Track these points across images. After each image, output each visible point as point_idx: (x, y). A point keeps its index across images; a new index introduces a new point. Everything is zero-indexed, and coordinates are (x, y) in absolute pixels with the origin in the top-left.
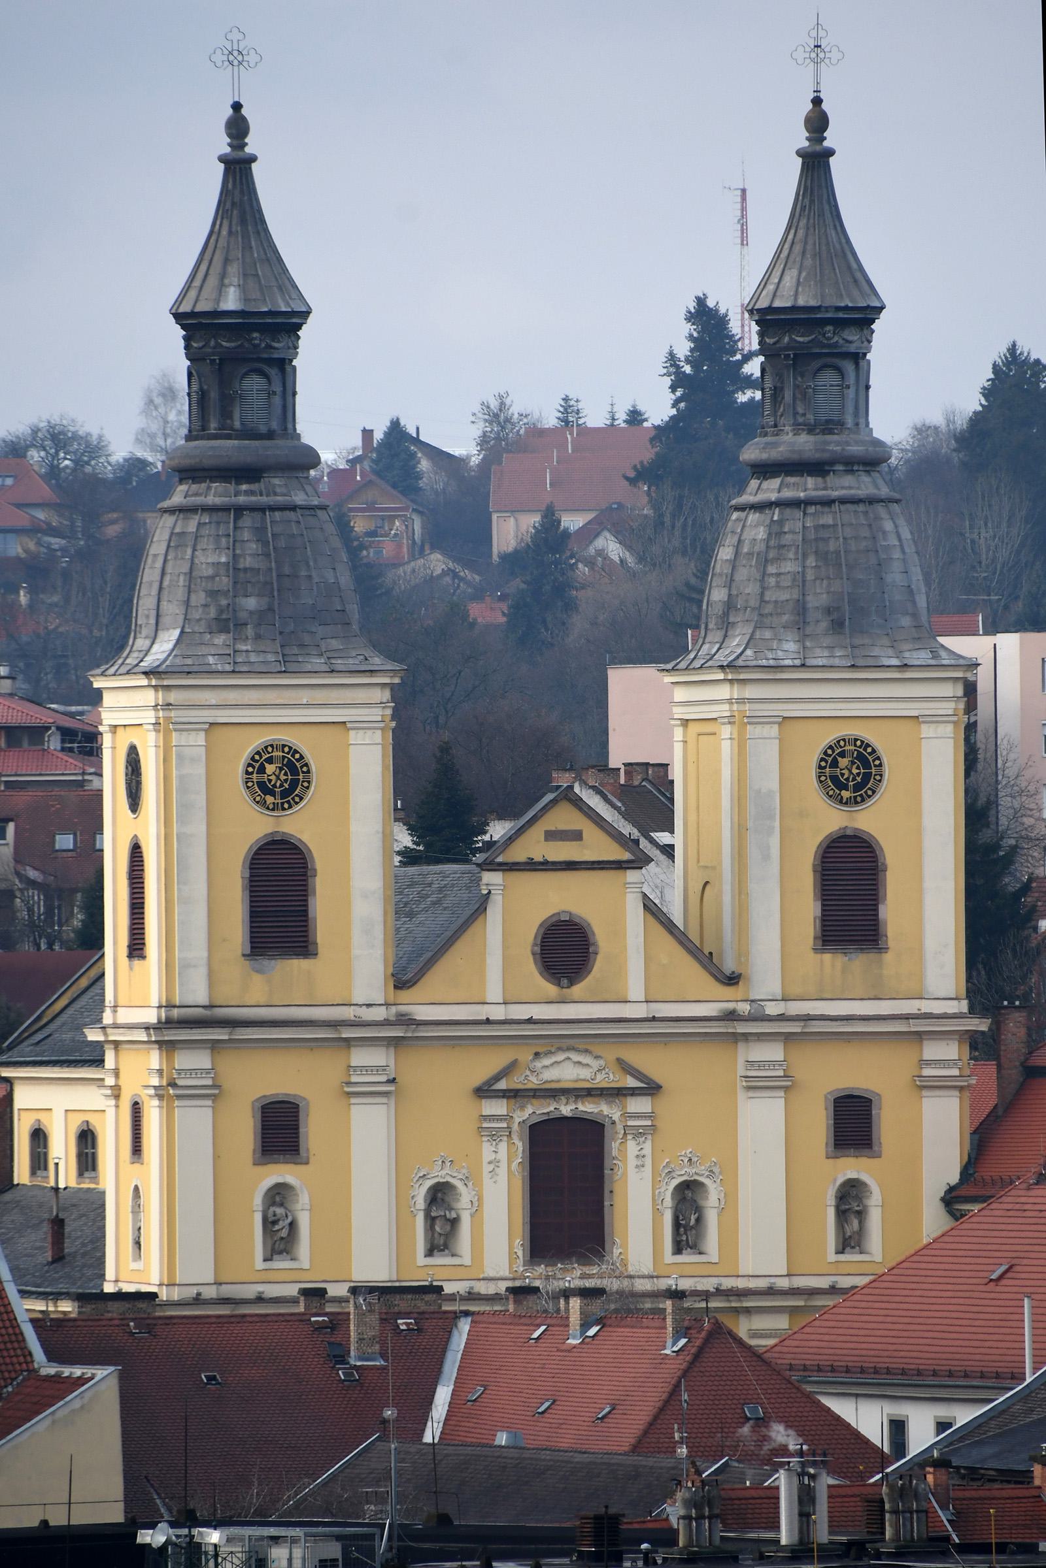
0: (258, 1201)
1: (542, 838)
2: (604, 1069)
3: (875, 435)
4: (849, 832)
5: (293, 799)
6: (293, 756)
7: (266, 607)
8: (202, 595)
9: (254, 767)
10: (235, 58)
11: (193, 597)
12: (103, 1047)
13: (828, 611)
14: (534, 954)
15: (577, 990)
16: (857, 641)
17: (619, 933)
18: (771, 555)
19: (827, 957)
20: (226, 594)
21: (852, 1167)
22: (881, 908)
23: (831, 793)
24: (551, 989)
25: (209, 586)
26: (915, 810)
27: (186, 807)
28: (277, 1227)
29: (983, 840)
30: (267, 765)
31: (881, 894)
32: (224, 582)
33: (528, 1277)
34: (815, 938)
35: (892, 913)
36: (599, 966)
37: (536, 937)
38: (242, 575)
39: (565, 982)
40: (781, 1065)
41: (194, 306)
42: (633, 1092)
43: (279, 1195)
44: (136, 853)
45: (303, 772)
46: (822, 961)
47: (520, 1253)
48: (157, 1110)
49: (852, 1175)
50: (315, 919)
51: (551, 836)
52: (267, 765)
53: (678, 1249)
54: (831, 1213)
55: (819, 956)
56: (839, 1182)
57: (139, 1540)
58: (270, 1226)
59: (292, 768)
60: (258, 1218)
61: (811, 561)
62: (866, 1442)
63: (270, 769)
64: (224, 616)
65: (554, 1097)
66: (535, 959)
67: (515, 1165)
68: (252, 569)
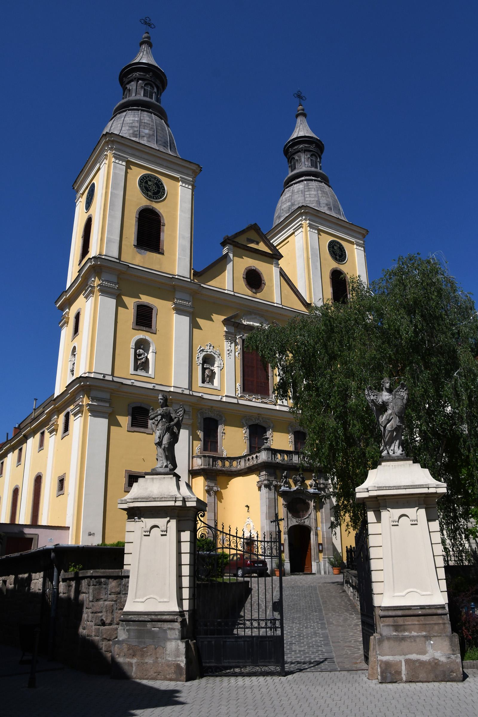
0: (132, 344)
7: (152, 134)
8: (127, 128)
10: (147, 23)
11: (123, 128)
13: (327, 205)
14: (243, 278)
17: (271, 280)
18: (306, 190)
20: (137, 127)
21: (141, 335)
23: (144, 192)
24: (249, 292)
25: (130, 125)
28: (140, 357)
29: (33, 590)
30: (149, 181)
32: (137, 124)
36: (265, 288)
38: (143, 124)
39: (254, 290)
41: (110, 130)
43: (142, 345)
44: (38, 480)
47: (239, 389)
48: (122, 631)
49: (141, 336)
50: (163, 241)
52: (149, 181)
58: (137, 356)
60: (132, 352)
61: (319, 192)
62: (201, 500)
63: (149, 183)
64: (136, 133)
66: (244, 280)
67: (237, 353)
68: (147, 123)
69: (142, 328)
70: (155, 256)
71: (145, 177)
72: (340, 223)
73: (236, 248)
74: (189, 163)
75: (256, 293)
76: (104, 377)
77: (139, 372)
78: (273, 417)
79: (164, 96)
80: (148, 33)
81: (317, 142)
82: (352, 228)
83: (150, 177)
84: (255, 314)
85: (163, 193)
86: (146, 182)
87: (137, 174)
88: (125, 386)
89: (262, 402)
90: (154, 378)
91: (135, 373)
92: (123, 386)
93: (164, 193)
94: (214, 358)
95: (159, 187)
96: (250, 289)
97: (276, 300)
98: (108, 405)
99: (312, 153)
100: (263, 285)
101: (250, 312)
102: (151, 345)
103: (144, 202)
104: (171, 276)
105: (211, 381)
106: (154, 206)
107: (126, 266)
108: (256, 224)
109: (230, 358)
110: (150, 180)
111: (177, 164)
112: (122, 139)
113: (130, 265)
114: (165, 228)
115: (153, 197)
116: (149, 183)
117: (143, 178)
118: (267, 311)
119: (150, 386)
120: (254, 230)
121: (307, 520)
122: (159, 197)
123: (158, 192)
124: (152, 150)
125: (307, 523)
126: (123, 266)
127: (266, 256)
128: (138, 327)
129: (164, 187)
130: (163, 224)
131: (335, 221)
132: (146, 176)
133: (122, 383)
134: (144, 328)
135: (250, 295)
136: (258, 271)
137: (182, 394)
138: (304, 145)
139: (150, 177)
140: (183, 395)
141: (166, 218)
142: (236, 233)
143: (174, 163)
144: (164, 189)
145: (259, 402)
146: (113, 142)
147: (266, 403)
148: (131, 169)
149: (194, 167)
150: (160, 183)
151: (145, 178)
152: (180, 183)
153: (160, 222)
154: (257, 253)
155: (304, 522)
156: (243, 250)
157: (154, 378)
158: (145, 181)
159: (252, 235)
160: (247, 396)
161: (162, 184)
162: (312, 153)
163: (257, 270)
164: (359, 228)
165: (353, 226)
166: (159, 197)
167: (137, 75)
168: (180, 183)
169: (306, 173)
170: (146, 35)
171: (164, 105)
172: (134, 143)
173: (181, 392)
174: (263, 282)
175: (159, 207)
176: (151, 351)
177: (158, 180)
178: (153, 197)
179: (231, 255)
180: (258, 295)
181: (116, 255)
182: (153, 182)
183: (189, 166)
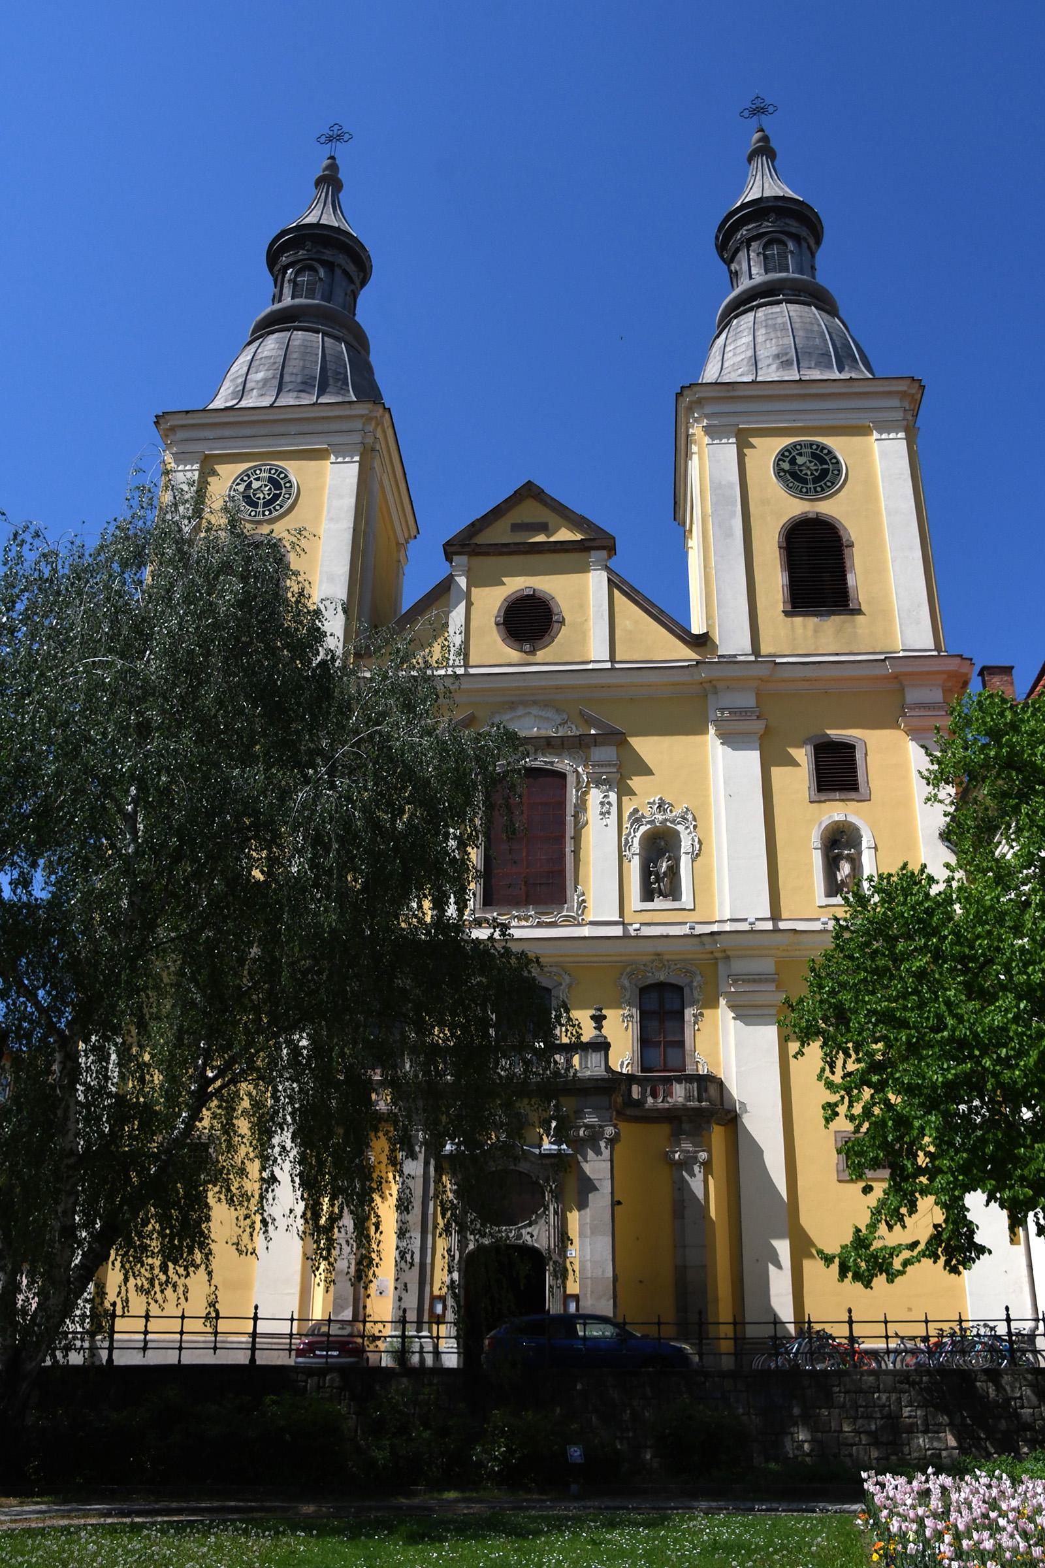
1: (509, 529)
2: (566, 722)
3: (358, 318)
5: (825, 484)
6: (278, 476)
9: (282, 479)
12: (956, 1555)
13: (777, 356)
14: (497, 624)
17: (582, 606)
19: (798, 620)
21: (837, 811)
22: (786, 581)
23: (791, 485)
24: (514, 655)
30: (797, 457)
33: (138, 688)
34: (784, 602)
35: (858, 579)
37: (499, 611)
39: (527, 647)
40: (754, 712)
42: (596, 741)
45: (790, 453)
46: (792, 623)
49: (838, 817)
52: (797, 457)
53: (648, 894)
56: (823, 826)
66: (499, 631)
69: (832, 795)
70: (833, 623)
71: (788, 450)
72: (813, 390)
74: (348, 406)
75: (532, 652)
76: (692, 928)
77: (658, 903)
78: (568, 959)
80: (762, 130)
81: (780, 204)
83: (798, 447)
84: (524, 703)
85: (836, 472)
87: (768, 450)
88: (805, 935)
89: (540, 925)
90: (693, 910)
93: (840, 471)
94: (677, 833)
95: (823, 462)
96: (516, 645)
97: (597, 650)
98: (772, 987)
99: (765, 239)
101: (513, 703)
102: (863, 833)
103: (796, 507)
104: (882, 657)
105: (674, 893)
106: (819, 511)
107: (766, 665)
109: (607, 825)
110: (800, 454)
111: (323, 418)
112: (189, 415)
113: (778, 660)
115: (815, 488)
116: (800, 460)
117: (783, 455)
118: (557, 688)
120: (533, 497)
122: (829, 484)
123: (825, 473)
124: (258, 411)
126: (679, 671)
127: (567, 551)
128: (823, 797)
129: (835, 457)
130: (848, 543)
131: (796, 390)
132: (789, 448)
133: (667, 936)
134: (837, 795)
136: (541, 595)
137: (752, 931)
138: (745, 228)
139: (798, 447)
140: (641, 940)
142: (473, 524)
143: (315, 419)
145: (531, 927)
146: (700, 402)
150: (825, 451)
151: (786, 454)
152: (876, 435)
153: (838, 539)
156: (501, 558)
157: (693, 910)
158: (282, 482)
159: (529, 511)
161: (830, 452)
162: (765, 239)
163: (538, 594)
164: (894, 382)
165: (856, 384)
166: (829, 484)
167: (745, 233)
168: (876, 435)
169: (745, 297)
170: (757, 136)
174: (555, 618)
176: (864, 844)
177: (818, 446)
178: (815, 488)
179: (462, 581)
180: (541, 655)
182: (806, 455)
183: (353, 412)
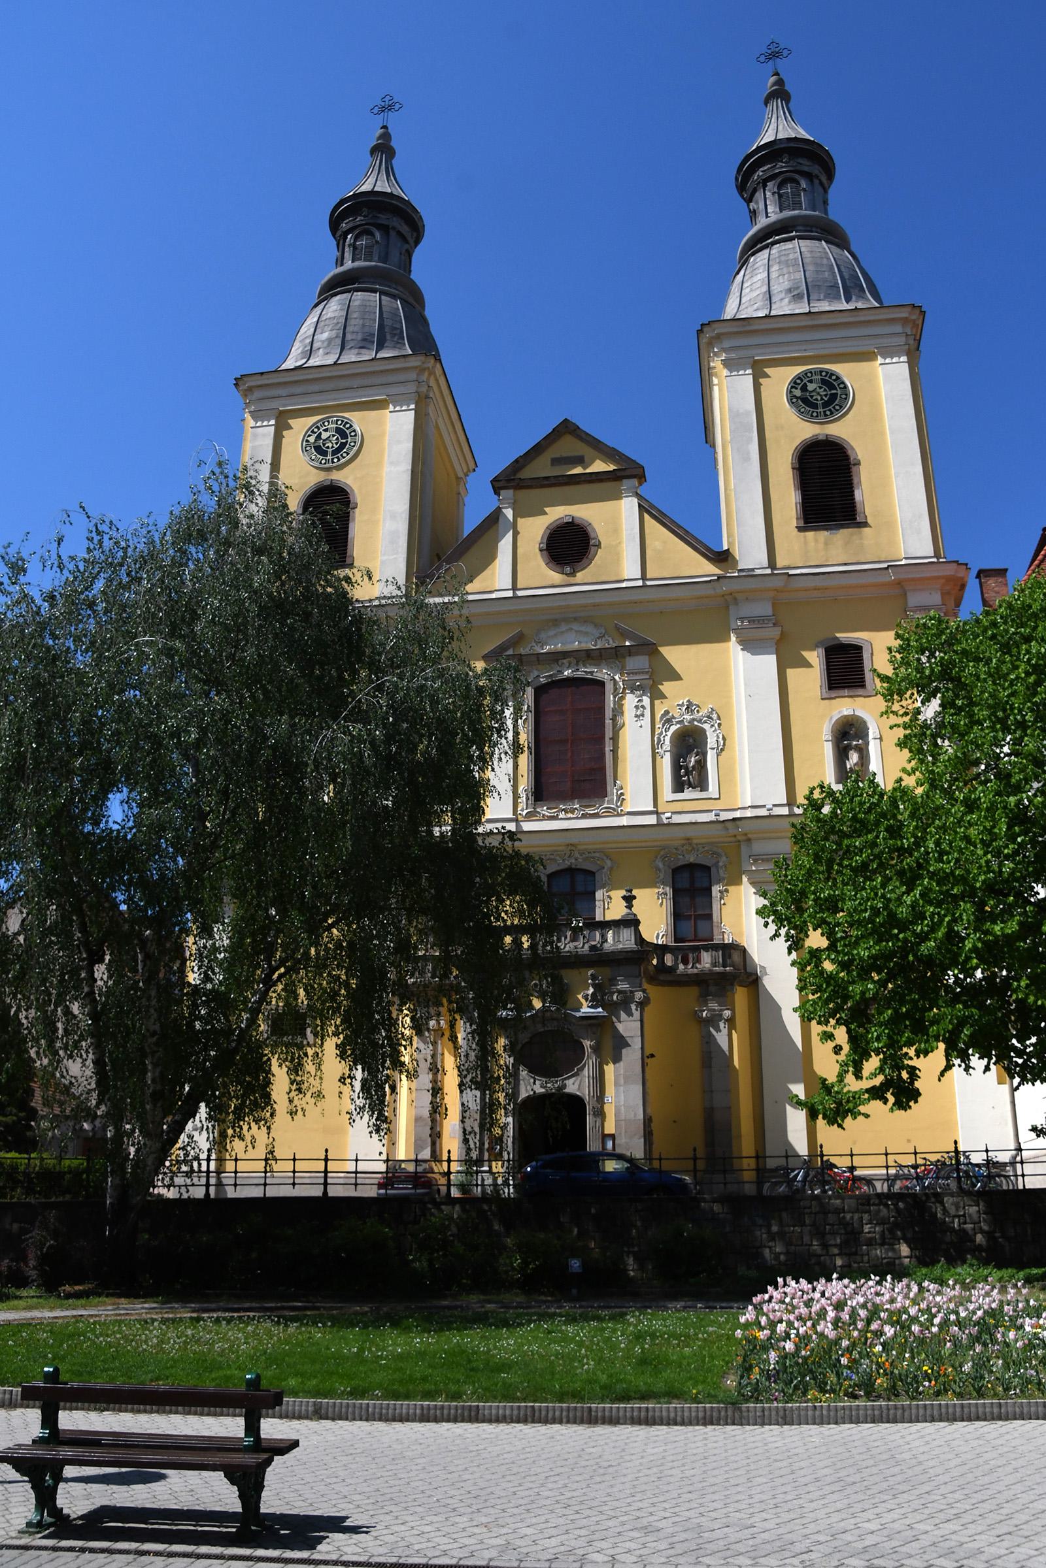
1: (549, 462)
4: (821, 438)
13: (789, 290)
14: (541, 550)
15: (580, 576)
16: (445, 1157)
19: (810, 535)
21: (846, 706)
24: (556, 577)
26: (876, 416)
27: (463, 1361)
31: (855, 481)
35: (865, 494)
36: (600, 557)
39: (568, 569)
42: (630, 651)
51: (556, 462)
53: (679, 787)
54: (828, 750)
55: (802, 534)
56: (834, 720)
57: (580, 1271)
59: (341, 433)
65: (557, 661)
73: (522, 493)
75: (573, 574)
77: (688, 794)
79: (835, 192)
81: (792, 145)
82: (862, 319)
84: (566, 620)
86: (804, 388)
89: (584, 816)
91: (680, 796)
92: (738, 823)
93: (847, 395)
94: (704, 731)
95: (832, 387)
99: (779, 180)
100: (593, 549)
104: (885, 565)
108: (566, 420)
110: (811, 381)
112: (264, 376)
113: (792, 572)
114: (357, 511)
116: (811, 387)
119: (710, 817)
121: (572, 1080)
123: (833, 397)
125: (572, 1086)
127: (601, 481)
128: (834, 694)
129: (843, 383)
135: (557, 582)
141: (860, 449)
143: (374, 373)
144: (846, 387)
145: (577, 818)
147: (595, 816)
148: (768, 376)
149: (904, 313)
152: (880, 360)
154: (578, 483)
155: (565, 1086)
160: (544, 810)
161: (838, 378)
162: (779, 180)
163: (576, 522)
164: (897, 310)
165: (861, 313)
168: (880, 360)
169: (761, 234)
171: (835, 214)
172: (394, 361)
173: (713, 818)
174: (592, 542)
175: (346, 477)
181: (763, 559)
182: (816, 381)
